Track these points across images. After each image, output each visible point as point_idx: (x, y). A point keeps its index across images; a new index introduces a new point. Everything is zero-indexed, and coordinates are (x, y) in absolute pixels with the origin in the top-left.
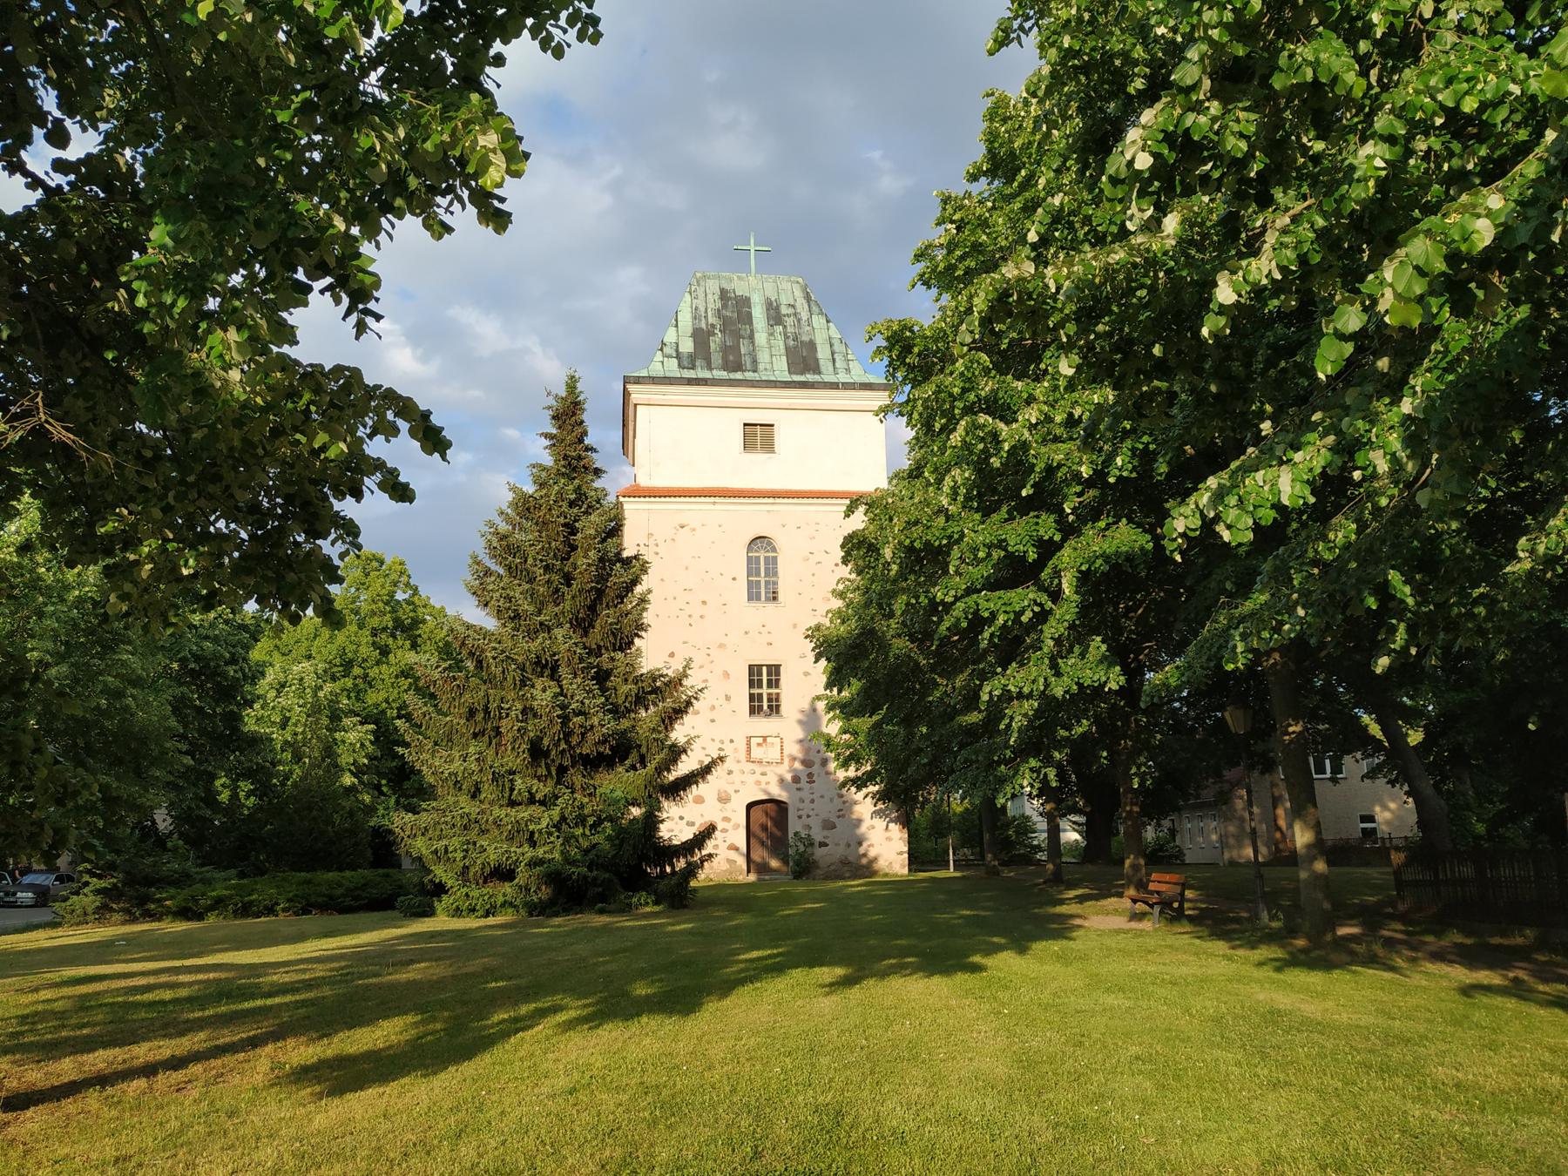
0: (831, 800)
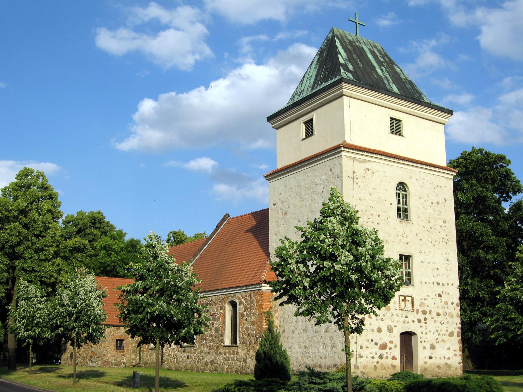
0: (434, 333)
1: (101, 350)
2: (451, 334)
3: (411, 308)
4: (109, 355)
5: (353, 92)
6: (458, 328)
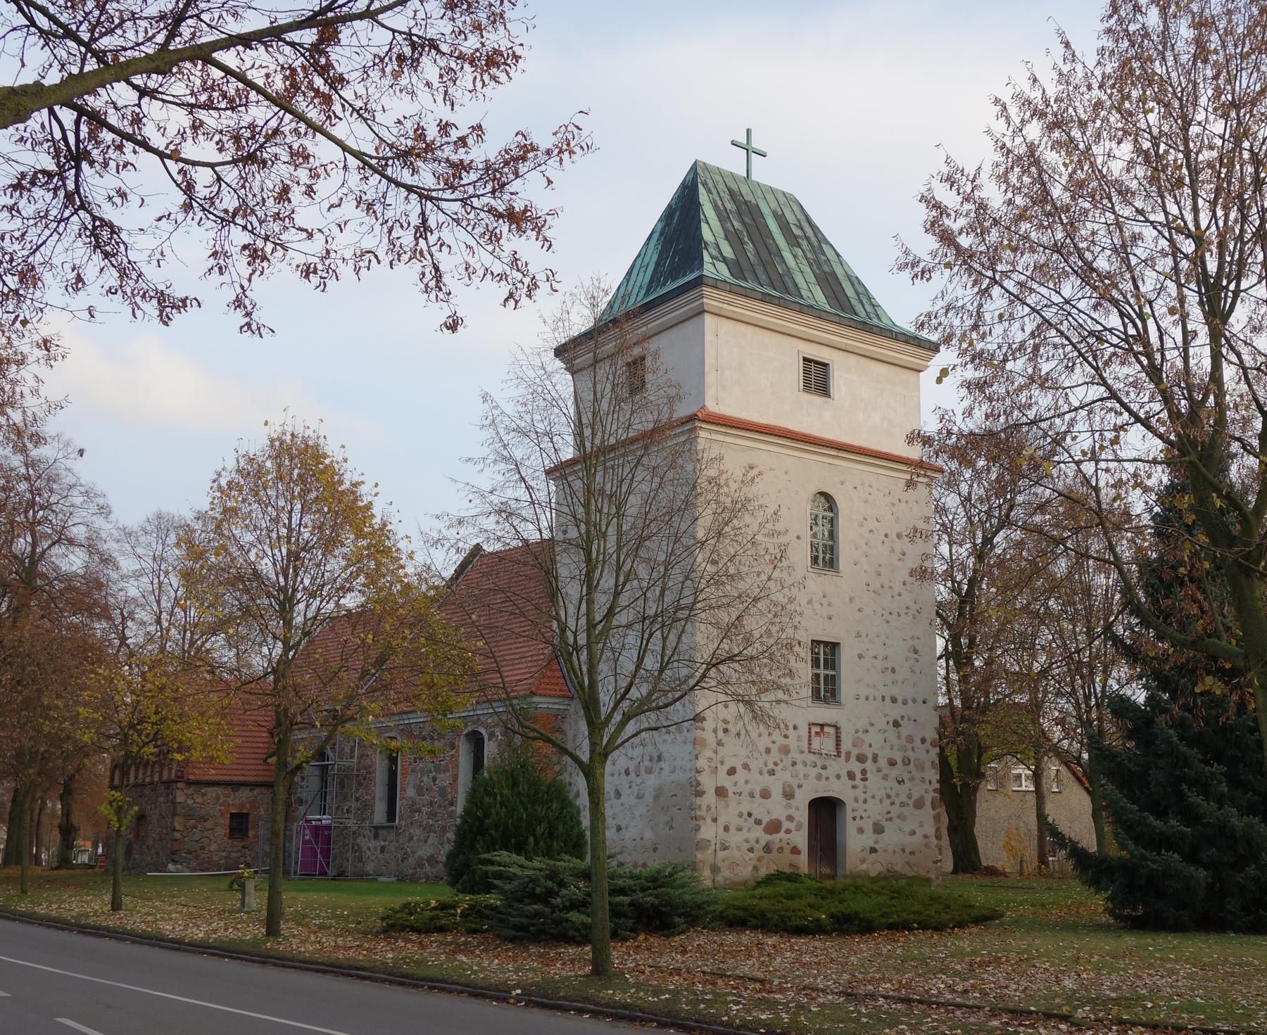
0: (881, 801)
1: (196, 837)
2: (919, 804)
4: (213, 847)
5: (726, 306)
6: (935, 791)
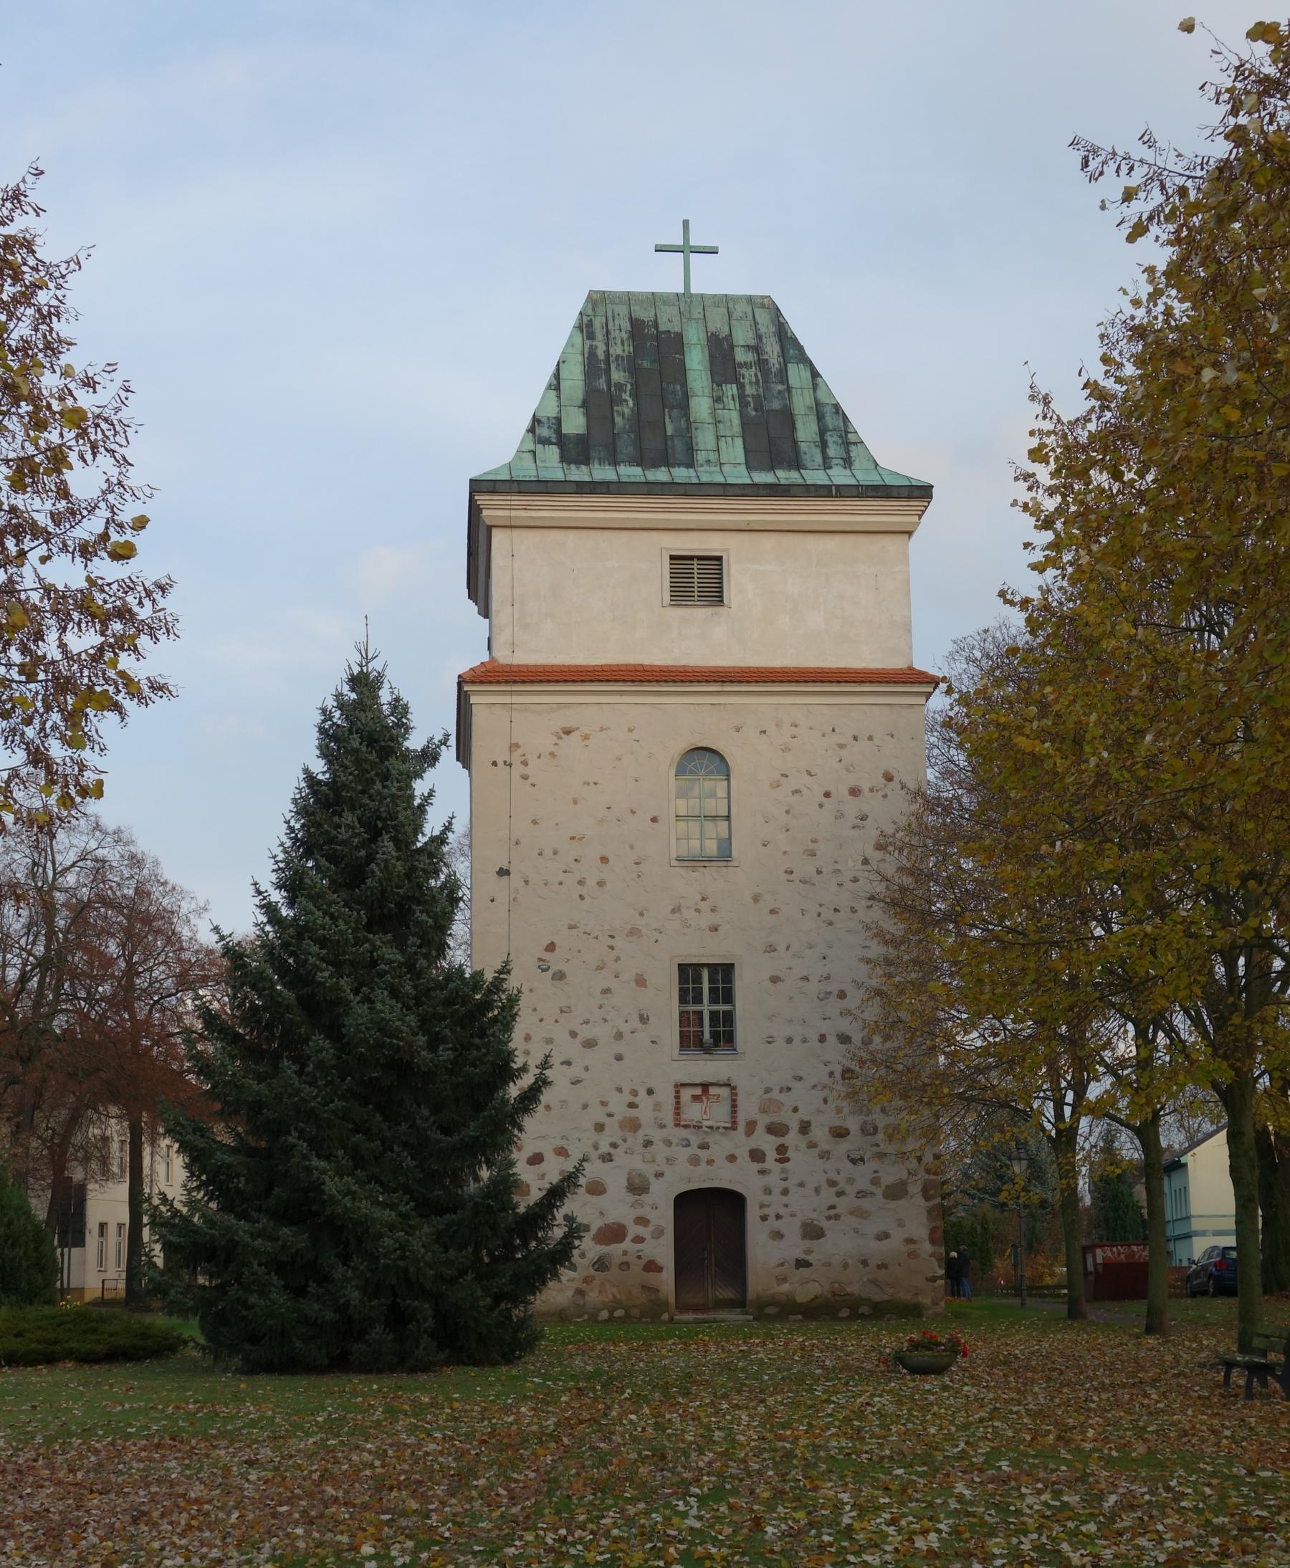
3: (729, 1119)
5: (514, 513)
